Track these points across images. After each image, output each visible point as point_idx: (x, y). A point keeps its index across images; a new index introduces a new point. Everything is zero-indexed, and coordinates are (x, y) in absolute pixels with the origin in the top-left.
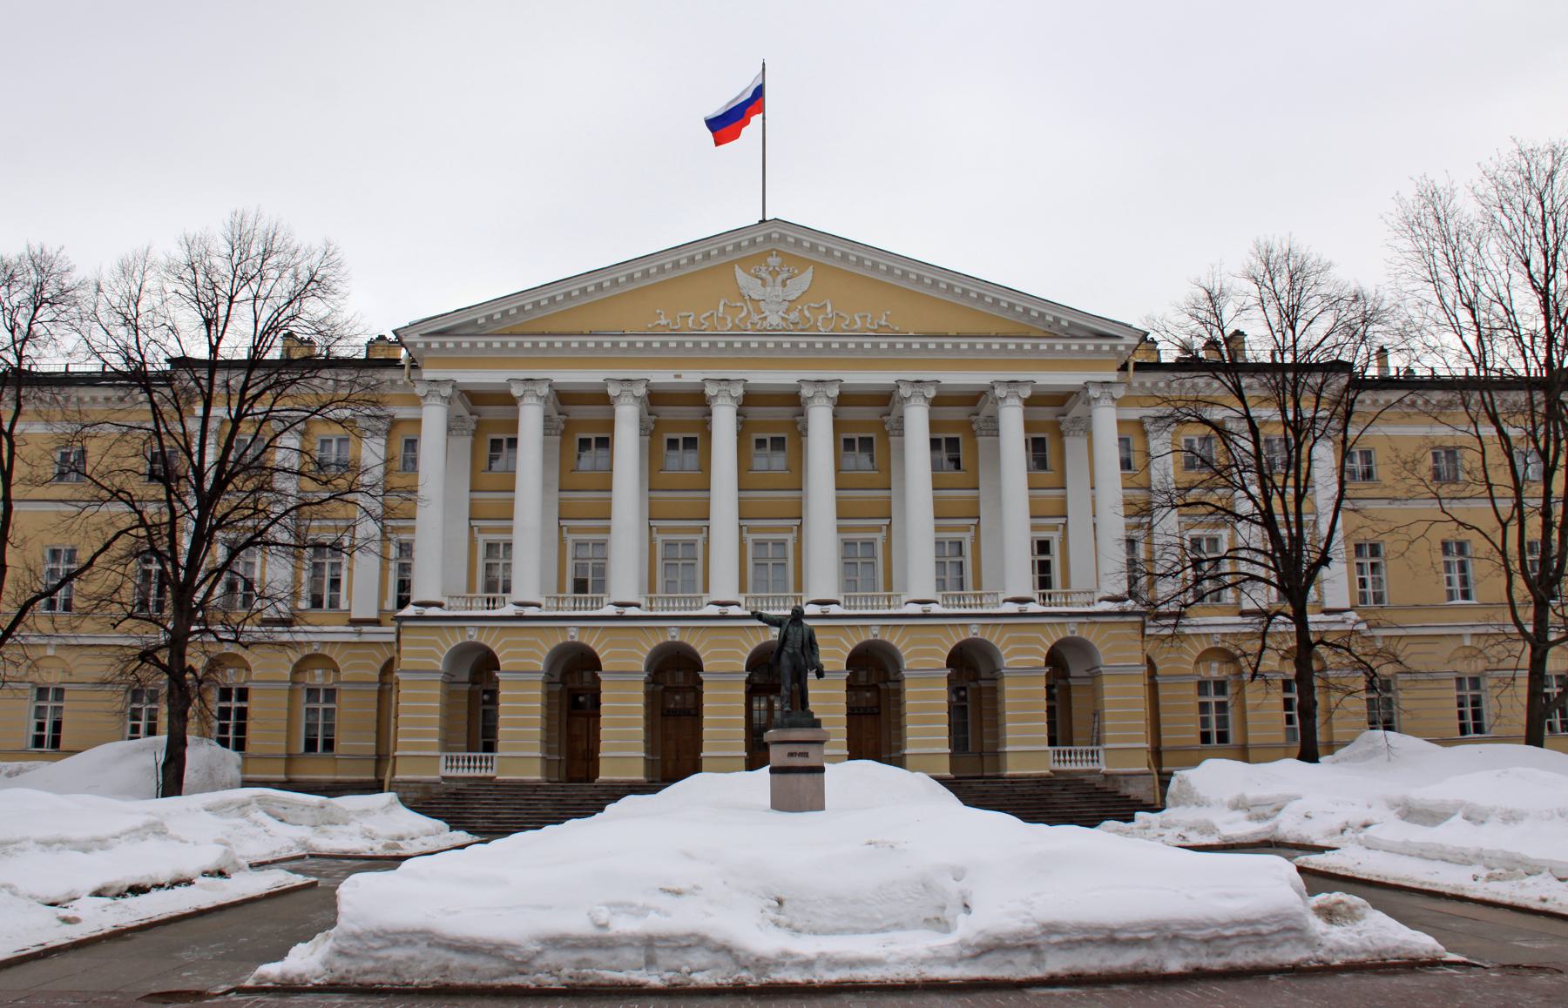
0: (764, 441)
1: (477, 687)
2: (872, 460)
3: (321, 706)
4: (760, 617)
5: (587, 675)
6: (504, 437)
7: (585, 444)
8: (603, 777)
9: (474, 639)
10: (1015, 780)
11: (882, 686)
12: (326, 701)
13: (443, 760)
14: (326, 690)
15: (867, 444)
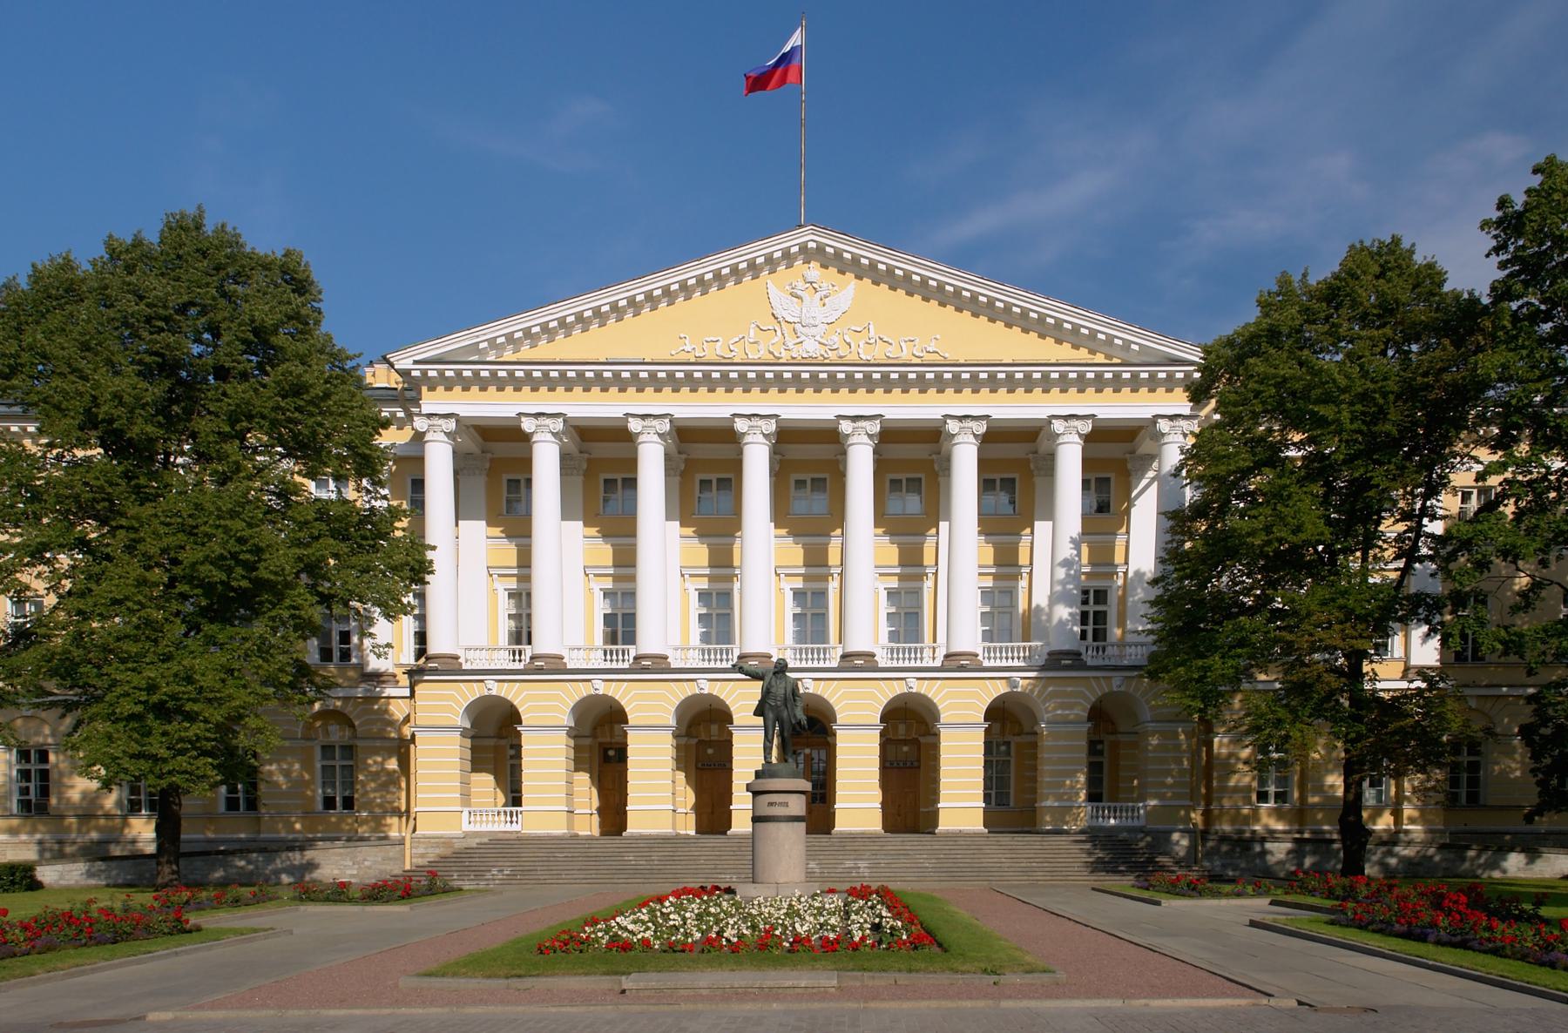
0: (804, 482)
1: (503, 742)
2: (1012, 502)
3: (338, 763)
4: (741, 670)
5: (714, 728)
6: (619, 477)
7: (705, 484)
8: (632, 829)
9: (494, 693)
10: (736, 836)
11: (922, 740)
12: (343, 758)
13: (465, 814)
14: (342, 747)
15: (1008, 485)
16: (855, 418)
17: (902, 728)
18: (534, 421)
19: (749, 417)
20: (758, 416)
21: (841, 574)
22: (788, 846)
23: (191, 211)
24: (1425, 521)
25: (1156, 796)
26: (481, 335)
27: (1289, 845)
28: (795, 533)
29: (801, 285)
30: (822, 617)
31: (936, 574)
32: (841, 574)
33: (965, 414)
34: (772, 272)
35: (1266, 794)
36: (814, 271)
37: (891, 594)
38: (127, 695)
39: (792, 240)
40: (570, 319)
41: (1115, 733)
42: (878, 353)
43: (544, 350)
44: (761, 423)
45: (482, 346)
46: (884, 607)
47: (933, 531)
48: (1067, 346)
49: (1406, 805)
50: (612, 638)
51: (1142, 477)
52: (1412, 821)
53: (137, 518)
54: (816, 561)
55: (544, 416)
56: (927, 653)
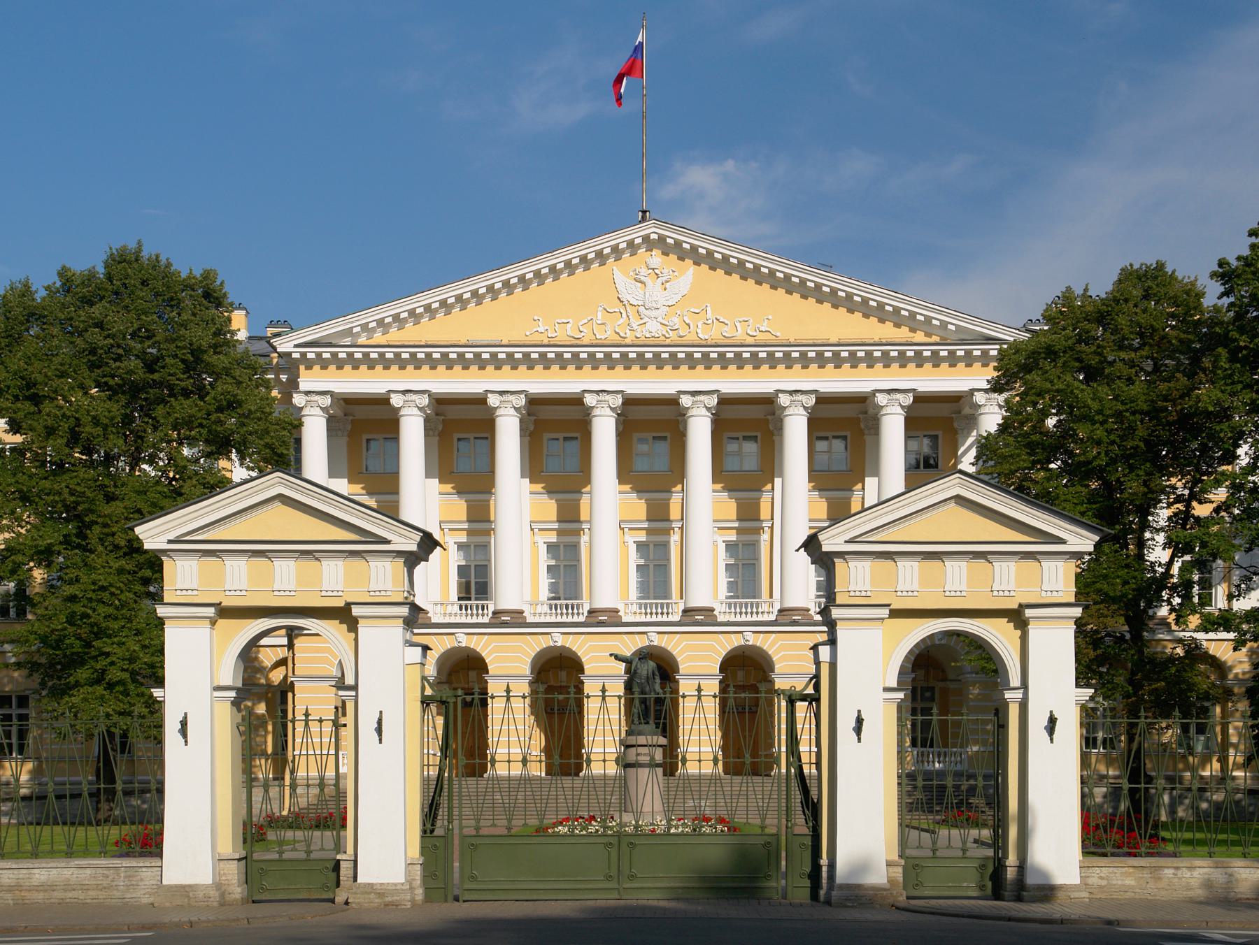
16: (695, 393)
17: (740, 675)
18: (401, 397)
19: (598, 392)
20: (603, 391)
21: (681, 528)
22: (649, 791)
23: (132, 246)
24: (1194, 504)
25: (976, 742)
26: (355, 321)
27: (1105, 789)
28: (639, 490)
29: (644, 271)
30: (664, 568)
31: (772, 528)
32: (681, 528)
33: (795, 389)
34: (618, 259)
35: (1095, 739)
36: (656, 258)
37: (730, 546)
38: (113, 663)
39: (635, 234)
40: (435, 305)
41: (945, 679)
42: (713, 333)
43: (411, 333)
44: (608, 397)
45: (355, 330)
46: (723, 558)
47: (769, 486)
48: (889, 325)
49: (1232, 751)
50: (465, 593)
51: (968, 435)
52: (1237, 766)
53: (109, 516)
54: (659, 517)
55: (410, 392)
56: (765, 608)
